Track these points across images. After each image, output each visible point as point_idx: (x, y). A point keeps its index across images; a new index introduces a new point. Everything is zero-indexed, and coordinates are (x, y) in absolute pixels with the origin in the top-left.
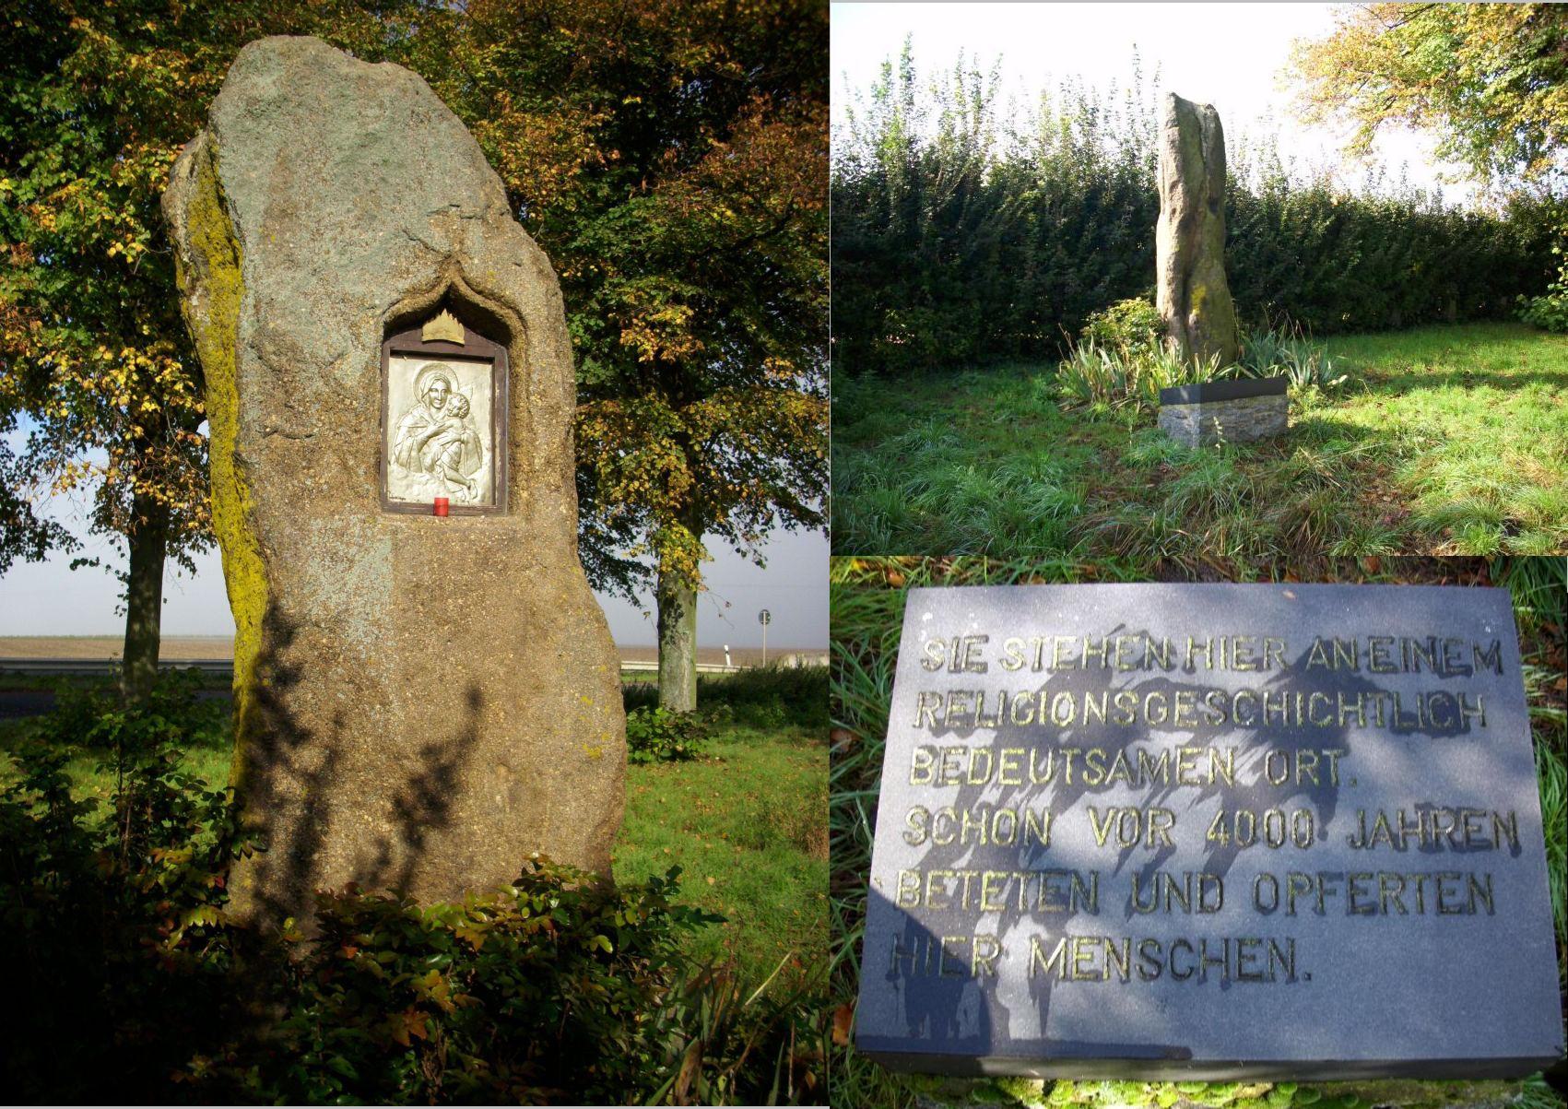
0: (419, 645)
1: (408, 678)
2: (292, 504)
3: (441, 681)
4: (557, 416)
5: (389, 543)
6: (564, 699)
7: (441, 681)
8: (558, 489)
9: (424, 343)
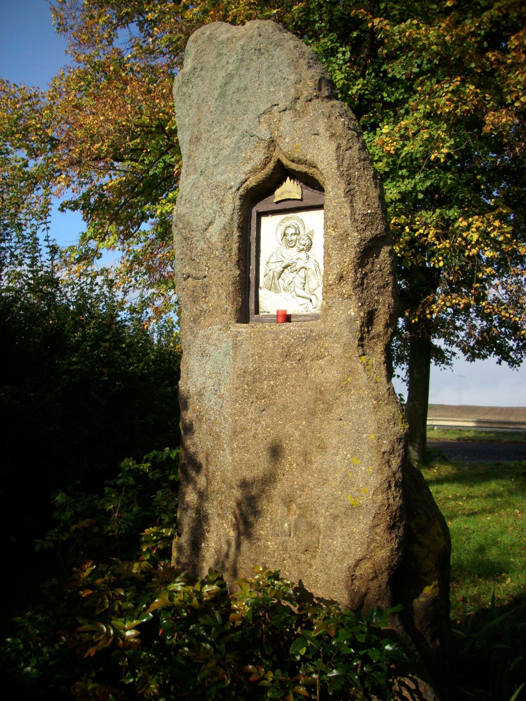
0: (242, 412)
1: (235, 433)
2: (194, 321)
3: (255, 437)
4: (347, 241)
5: (231, 344)
6: (338, 458)
7: (255, 437)
8: (349, 297)
9: (277, 203)
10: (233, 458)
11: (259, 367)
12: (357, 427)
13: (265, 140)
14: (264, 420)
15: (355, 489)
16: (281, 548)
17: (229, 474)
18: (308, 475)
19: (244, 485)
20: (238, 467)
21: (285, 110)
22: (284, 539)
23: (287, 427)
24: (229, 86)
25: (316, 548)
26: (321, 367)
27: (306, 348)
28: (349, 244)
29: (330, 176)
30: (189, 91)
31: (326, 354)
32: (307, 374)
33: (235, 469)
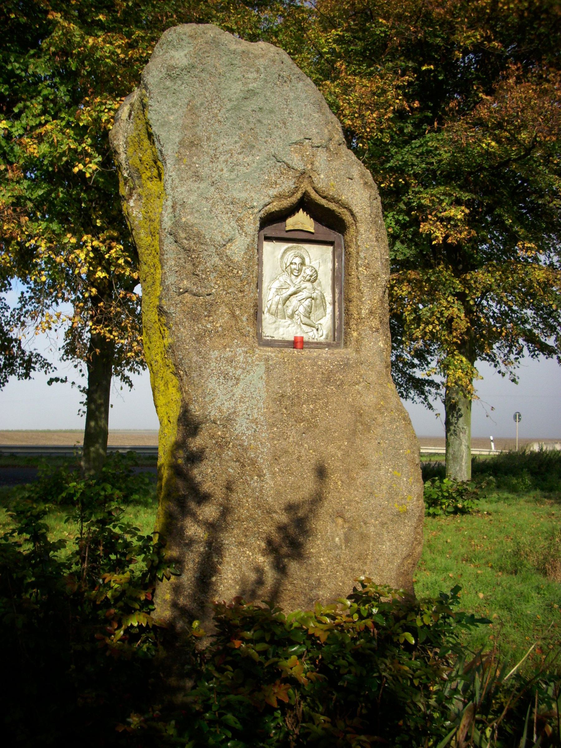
0: (283, 436)
1: (276, 459)
3: (299, 460)
6: (382, 472)
7: (299, 460)
8: (377, 330)
9: (287, 231)
10: (276, 482)
11: (298, 391)
12: (393, 444)
13: (296, 170)
14: (307, 443)
15: (400, 497)
16: (334, 561)
17: (270, 499)
18: (354, 490)
19: (290, 508)
20: (282, 491)
21: (318, 147)
22: (336, 552)
23: (329, 447)
24: (247, 103)
25: (367, 555)
26: (359, 393)
27: (344, 375)
28: (378, 283)
29: (363, 220)
30: (176, 87)
31: (361, 380)
32: (346, 398)
33: (278, 493)
